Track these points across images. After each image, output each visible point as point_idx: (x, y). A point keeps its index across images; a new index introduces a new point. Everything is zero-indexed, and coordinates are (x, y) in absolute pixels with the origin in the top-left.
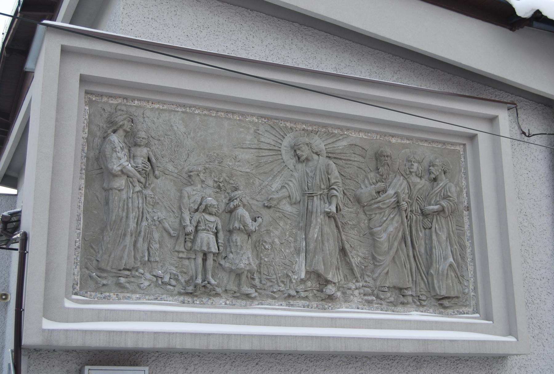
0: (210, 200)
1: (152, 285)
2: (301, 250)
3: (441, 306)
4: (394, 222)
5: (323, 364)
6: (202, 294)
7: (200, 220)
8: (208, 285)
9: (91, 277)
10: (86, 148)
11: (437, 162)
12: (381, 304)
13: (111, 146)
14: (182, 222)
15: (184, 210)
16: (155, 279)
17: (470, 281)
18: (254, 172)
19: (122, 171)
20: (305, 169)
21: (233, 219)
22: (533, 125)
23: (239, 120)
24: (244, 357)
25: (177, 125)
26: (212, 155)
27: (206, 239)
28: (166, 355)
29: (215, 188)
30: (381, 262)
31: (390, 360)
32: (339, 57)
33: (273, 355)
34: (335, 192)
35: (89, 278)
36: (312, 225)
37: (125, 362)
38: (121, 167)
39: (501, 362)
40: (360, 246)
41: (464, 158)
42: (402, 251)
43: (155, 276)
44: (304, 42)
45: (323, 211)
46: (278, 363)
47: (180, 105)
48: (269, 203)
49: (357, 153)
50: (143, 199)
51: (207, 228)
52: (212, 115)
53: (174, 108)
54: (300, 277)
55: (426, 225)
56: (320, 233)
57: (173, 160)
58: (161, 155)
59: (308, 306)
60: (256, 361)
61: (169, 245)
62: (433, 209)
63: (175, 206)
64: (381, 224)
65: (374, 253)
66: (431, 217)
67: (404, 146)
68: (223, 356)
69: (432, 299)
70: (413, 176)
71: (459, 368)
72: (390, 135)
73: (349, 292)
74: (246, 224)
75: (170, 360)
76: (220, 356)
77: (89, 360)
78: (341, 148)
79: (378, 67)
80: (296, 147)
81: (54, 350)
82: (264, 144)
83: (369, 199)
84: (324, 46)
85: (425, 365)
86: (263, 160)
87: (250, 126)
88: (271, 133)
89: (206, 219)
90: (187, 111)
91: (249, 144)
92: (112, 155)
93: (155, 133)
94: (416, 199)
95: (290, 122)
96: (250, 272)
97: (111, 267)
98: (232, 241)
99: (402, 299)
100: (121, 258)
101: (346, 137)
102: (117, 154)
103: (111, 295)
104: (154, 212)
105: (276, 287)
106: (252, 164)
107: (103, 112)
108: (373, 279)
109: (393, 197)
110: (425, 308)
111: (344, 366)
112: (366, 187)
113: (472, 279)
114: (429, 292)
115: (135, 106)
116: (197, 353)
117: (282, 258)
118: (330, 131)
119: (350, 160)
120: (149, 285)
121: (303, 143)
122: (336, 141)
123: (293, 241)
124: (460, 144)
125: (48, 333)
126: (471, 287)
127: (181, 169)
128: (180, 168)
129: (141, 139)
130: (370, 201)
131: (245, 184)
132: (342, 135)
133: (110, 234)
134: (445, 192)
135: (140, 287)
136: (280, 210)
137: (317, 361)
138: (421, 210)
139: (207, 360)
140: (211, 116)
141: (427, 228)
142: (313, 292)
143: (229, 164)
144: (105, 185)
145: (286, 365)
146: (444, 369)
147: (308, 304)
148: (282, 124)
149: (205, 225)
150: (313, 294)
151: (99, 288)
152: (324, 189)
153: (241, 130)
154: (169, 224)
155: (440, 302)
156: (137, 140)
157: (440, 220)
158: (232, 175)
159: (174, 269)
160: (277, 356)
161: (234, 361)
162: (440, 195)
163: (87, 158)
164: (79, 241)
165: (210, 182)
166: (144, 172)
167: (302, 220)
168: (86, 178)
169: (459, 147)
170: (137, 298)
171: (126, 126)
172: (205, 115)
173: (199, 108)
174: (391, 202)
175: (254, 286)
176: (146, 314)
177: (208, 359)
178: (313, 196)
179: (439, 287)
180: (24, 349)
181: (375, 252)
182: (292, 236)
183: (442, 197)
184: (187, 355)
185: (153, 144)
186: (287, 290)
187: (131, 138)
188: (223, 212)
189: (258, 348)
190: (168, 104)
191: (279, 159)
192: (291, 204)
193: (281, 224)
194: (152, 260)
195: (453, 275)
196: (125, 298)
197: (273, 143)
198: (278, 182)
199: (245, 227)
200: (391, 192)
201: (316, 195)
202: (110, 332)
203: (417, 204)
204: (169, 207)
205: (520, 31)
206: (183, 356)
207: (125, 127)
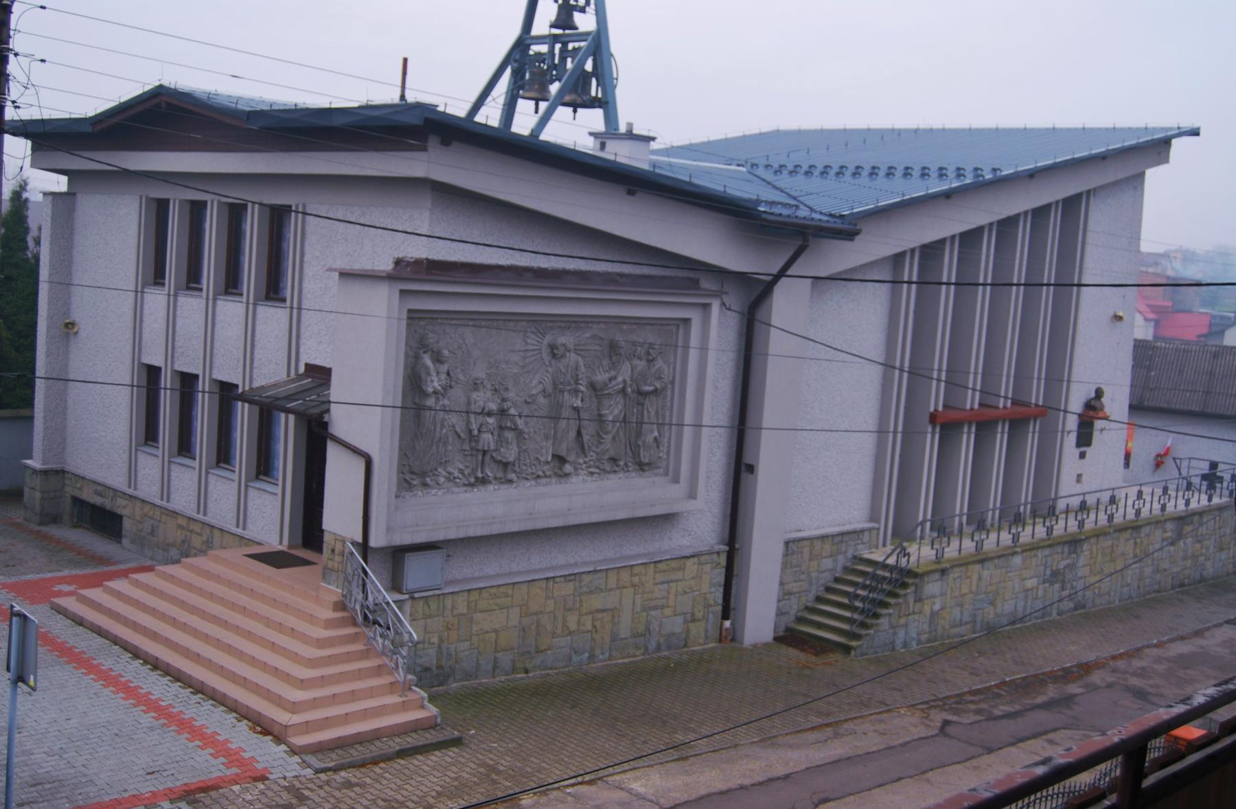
9: (405, 480)
86: (528, 360)
99: (617, 469)
192: (545, 397)
197: (536, 343)
200: (620, 379)
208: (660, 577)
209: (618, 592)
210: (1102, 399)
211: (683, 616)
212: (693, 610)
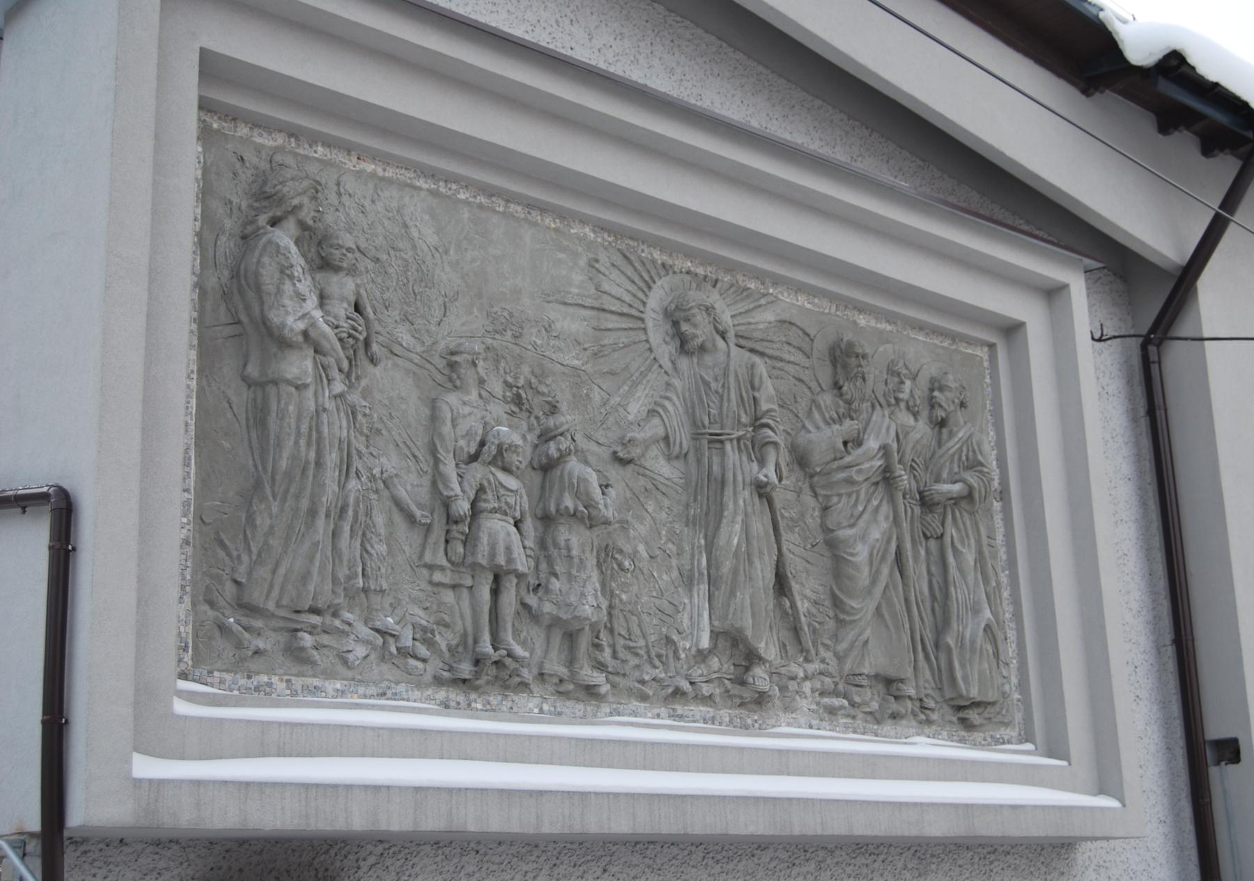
0: (505, 432)
1: (373, 656)
2: (697, 575)
3: (962, 723)
4: (881, 518)
5: (740, 867)
6: (488, 683)
7: (486, 484)
8: (508, 661)
9: (223, 628)
10: (198, 261)
11: (951, 381)
12: (854, 717)
13: (277, 259)
14: (441, 486)
15: (444, 454)
16: (380, 641)
17: (1012, 666)
18: (589, 368)
19: (305, 334)
20: (697, 369)
21: (556, 486)
22: (1095, 316)
23: (556, 230)
24: (577, 853)
25: (418, 224)
26: (499, 313)
27: (502, 536)
28: (400, 851)
29: (507, 402)
30: (853, 614)
31: (870, 855)
32: (746, 102)
33: (638, 846)
34: (770, 433)
35: (217, 633)
36: (726, 514)
37: (302, 872)
38: (306, 321)
39: (1066, 856)
40: (807, 572)
41: (991, 378)
42: (895, 587)
43: (378, 631)
44: (677, 55)
45: (748, 480)
46: (649, 867)
47: (432, 174)
48: (626, 451)
49: (794, 343)
50: (348, 415)
51: (505, 507)
52: (497, 209)
53: (410, 178)
54: (697, 645)
55: (930, 528)
56: (744, 536)
57: (410, 318)
58: (381, 301)
59: (713, 720)
60: (602, 863)
61: (407, 548)
62: (949, 492)
63: (418, 443)
64: (852, 521)
66: (940, 510)
67: (883, 338)
68: (531, 851)
69: (945, 706)
70: (901, 410)
71: (994, 871)
72: (855, 308)
73: (793, 685)
74: (592, 500)
75: (411, 863)
76: (524, 850)
77: (212, 869)
78: (761, 326)
79: (821, 140)
80: (678, 315)
81: (121, 841)
82: (609, 298)
83: (828, 458)
84: (716, 72)
85: (933, 867)
86: (608, 339)
87: (580, 249)
88: (623, 273)
89: (500, 483)
90: (441, 189)
91: (578, 295)
92: (281, 286)
93: (367, 240)
94: (911, 465)
95: (661, 251)
96: (594, 627)
97: (277, 603)
98: (556, 545)
99: (894, 706)
100: (305, 577)
101: (772, 302)
102: (294, 284)
103: (273, 681)
104: (371, 454)
105: (648, 668)
106: (586, 346)
107: (238, 165)
108: (836, 654)
109: (874, 457)
110: (934, 727)
111: (783, 872)
112: (818, 428)
113: (1015, 661)
114: (940, 689)
115: (317, 159)
116: (472, 845)
117: (654, 594)
118: (740, 282)
119: (781, 360)
120: (367, 656)
121: (699, 306)
122: (755, 308)
123: (675, 552)
124: (983, 343)
125: (149, 790)
126: (1014, 680)
127: (430, 343)
128: (428, 342)
129: (344, 251)
130: (828, 463)
131: (571, 399)
132: (764, 295)
133: (273, 508)
135: (345, 662)
136: (648, 472)
137: (730, 859)
138: (920, 493)
139: (496, 861)
140: (494, 211)
141: (932, 536)
142: (724, 685)
143: (535, 342)
144: (253, 371)
145: (666, 872)
146: (967, 875)
147: (712, 714)
148: (646, 252)
149: (498, 497)
150: (722, 690)
151: (243, 660)
152: (746, 426)
153: (562, 256)
154: (406, 491)
155: (961, 715)
156: (331, 254)
157: (962, 517)
158: (544, 371)
159: (421, 613)
160: (647, 848)
161: (555, 865)
162: (960, 459)
163: (201, 288)
164: (188, 524)
165: (496, 387)
166: (351, 341)
167: (695, 500)
168: (200, 345)
169: (981, 349)
170: (338, 690)
171: (305, 209)
172: (481, 206)
173: (468, 184)
174: (874, 469)
175: (600, 666)
176: (379, 736)
177: (497, 860)
178: (721, 442)
179: (965, 678)
180: (75, 842)
181: (840, 589)
182: (674, 541)
183: (963, 463)
184: (450, 849)
185: (363, 269)
186: (670, 677)
187: (309, 245)
188: (526, 467)
189: (648, 830)
190: (396, 164)
191: (640, 342)
192: (669, 458)
193: (651, 507)
194: (373, 587)
195: (991, 652)
196: (307, 689)
197: (628, 298)
198: (639, 398)
199: (591, 510)
200: (872, 444)
201: (727, 439)
202: (307, 788)
203: (912, 476)
204: (404, 442)
205: (1108, 98)
206: (440, 852)
207: (303, 214)
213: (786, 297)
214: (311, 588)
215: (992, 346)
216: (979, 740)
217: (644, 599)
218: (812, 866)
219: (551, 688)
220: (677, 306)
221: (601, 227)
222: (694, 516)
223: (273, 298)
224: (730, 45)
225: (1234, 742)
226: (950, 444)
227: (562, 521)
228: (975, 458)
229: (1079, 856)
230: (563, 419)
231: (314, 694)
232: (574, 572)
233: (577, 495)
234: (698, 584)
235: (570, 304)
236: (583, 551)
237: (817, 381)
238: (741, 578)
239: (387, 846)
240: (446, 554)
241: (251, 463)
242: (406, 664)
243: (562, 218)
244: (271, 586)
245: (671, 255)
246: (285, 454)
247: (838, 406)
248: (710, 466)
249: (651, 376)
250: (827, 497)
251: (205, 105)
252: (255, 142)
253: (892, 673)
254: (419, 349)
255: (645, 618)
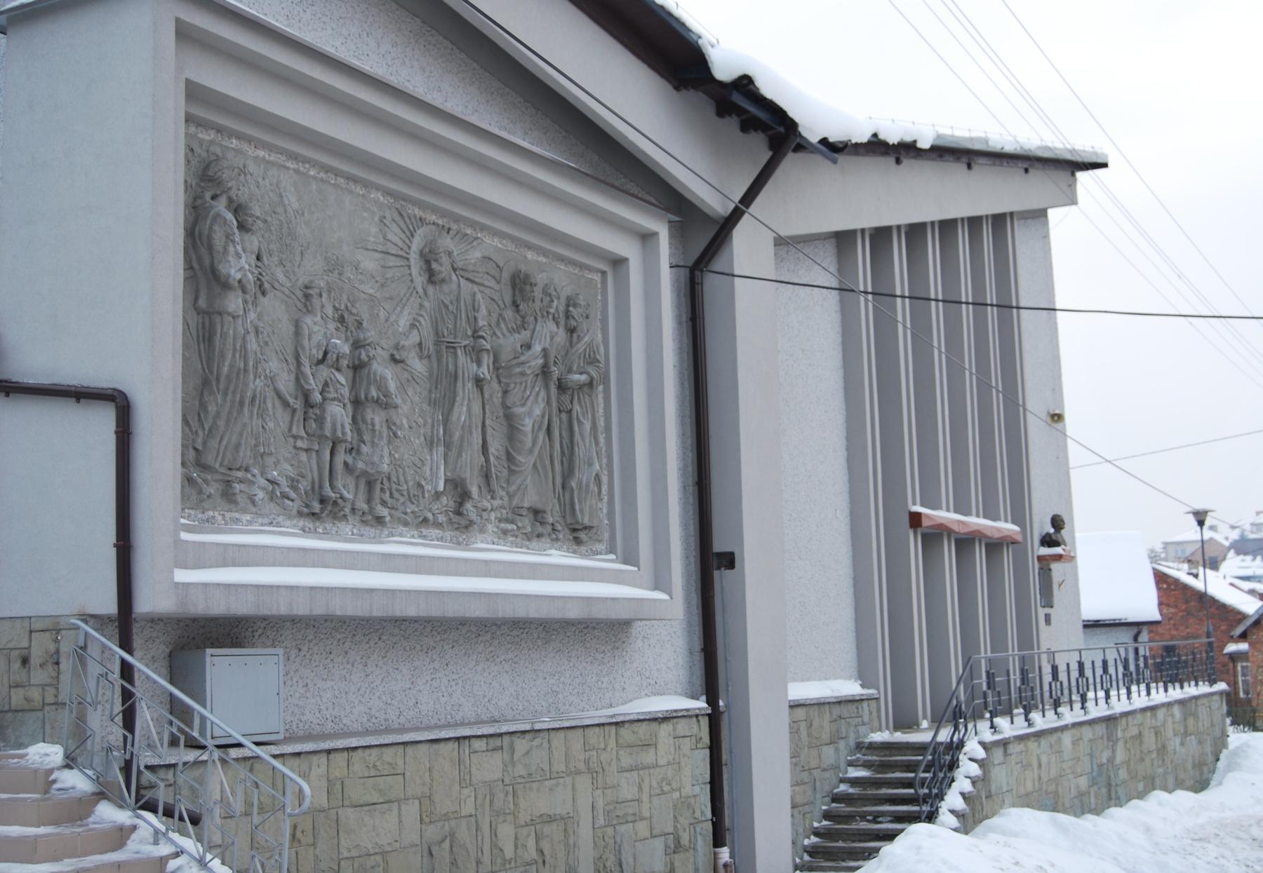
2: (436, 440)
4: (540, 400)
7: (329, 381)
8: (340, 501)
14: (302, 382)
16: (271, 488)
18: (378, 295)
19: (240, 281)
21: (365, 381)
23: (363, 196)
27: (339, 416)
29: (335, 321)
34: (485, 343)
36: (458, 399)
46: (403, 636)
47: (295, 157)
51: (340, 397)
54: (435, 488)
57: (284, 263)
62: (579, 381)
65: (511, 451)
66: (570, 392)
69: (566, 529)
72: (526, 246)
73: (485, 515)
85: (554, 637)
91: (374, 242)
98: (364, 421)
99: (540, 529)
105: (409, 504)
108: (508, 493)
110: (559, 543)
112: (504, 335)
115: (233, 148)
126: (605, 511)
134: (592, 353)
137: (445, 631)
140: (329, 182)
151: (201, 501)
153: (365, 214)
155: (575, 535)
156: (246, 220)
157: (584, 398)
159: (289, 468)
165: (329, 311)
167: (436, 388)
172: (322, 180)
177: (324, 631)
178: (454, 348)
179: (581, 511)
181: (513, 449)
192: (421, 358)
200: (537, 348)
208: (627, 760)
209: (569, 781)
210: (1063, 531)
211: (662, 838)
212: (675, 827)
213: (488, 240)
214: (241, 454)
215: (604, 273)
216: (584, 552)
217: (406, 457)
218: (488, 636)
219: (358, 518)
220: (430, 251)
221: (388, 192)
222: (435, 399)
223: (221, 255)
224: (458, 48)
225: (732, 554)
226: (579, 345)
227: (368, 405)
228: (595, 358)
229: (633, 630)
230: (369, 334)
231: (236, 524)
232: (376, 441)
233: (379, 389)
234: (437, 446)
235: (370, 250)
236: (382, 427)
237: (503, 300)
238: (466, 444)
239: (267, 622)
240: (304, 428)
241: (200, 366)
242: (284, 503)
243: (366, 186)
244: (218, 452)
245: (424, 212)
246: (227, 363)
247: (516, 319)
248: (447, 365)
249: (412, 299)
250: (507, 384)
251: (189, 119)
252: (198, 138)
253: (539, 506)
254: (288, 285)
255: (407, 469)
